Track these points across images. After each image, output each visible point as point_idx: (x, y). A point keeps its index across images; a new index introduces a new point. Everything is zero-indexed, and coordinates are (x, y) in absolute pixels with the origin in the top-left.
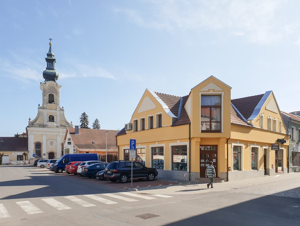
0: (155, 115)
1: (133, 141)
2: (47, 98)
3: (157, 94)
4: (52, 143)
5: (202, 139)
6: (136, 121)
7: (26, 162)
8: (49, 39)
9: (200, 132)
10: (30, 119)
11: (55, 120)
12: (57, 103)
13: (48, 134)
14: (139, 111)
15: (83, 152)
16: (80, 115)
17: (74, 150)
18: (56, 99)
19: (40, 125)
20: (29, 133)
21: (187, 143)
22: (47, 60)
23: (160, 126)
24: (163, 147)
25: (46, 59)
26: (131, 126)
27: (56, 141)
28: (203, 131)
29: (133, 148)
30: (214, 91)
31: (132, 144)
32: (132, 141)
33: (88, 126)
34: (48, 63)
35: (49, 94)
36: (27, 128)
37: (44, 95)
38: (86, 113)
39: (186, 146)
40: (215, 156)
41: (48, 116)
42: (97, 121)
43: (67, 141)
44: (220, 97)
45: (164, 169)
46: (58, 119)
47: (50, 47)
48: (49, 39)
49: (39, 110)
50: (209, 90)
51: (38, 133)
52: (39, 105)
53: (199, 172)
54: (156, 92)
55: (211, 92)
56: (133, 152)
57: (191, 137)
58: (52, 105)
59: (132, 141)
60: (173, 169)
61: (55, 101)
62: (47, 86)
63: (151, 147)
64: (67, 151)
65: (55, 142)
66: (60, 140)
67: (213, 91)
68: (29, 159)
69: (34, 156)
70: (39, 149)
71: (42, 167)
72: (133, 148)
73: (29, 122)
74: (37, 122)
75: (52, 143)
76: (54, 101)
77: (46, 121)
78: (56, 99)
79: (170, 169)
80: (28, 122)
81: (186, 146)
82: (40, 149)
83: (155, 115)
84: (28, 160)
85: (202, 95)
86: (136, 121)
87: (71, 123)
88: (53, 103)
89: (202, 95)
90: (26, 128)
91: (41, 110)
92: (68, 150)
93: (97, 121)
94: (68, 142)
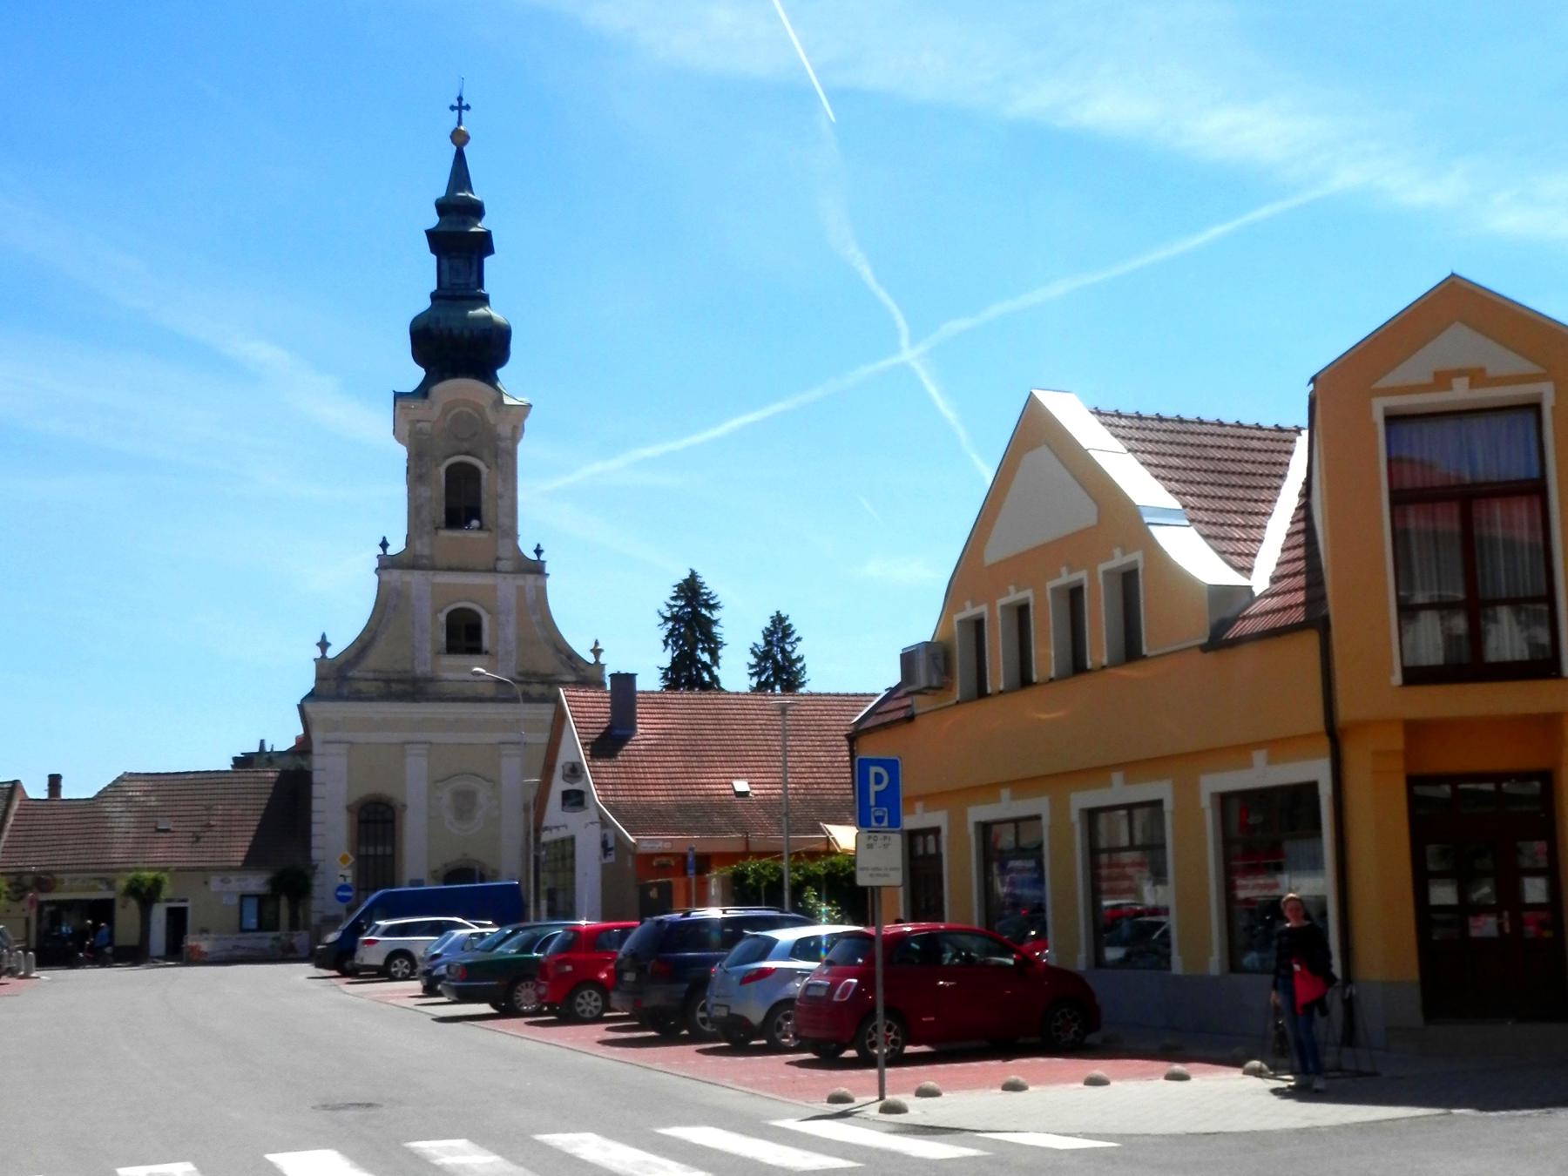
0: (1092, 577)
1: (881, 770)
2: (436, 490)
3: (1110, 418)
4: (465, 803)
5: (1415, 730)
6: (978, 624)
7: (295, 940)
8: (452, 108)
9: (1397, 678)
10: (324, 645)
11: (486, 642)
12: (504, 521)
13: (438, 737)
14: (992, 555)
15: (664, 860)
16: (661, 595)
17: (604, 844)
18: (499, 496)
19: (388, 681)
20: (317, 736)
21: (1317, 770)
22: (436, 239)
23: (1130, 650)
24: (1157, 804)
25: (431, 234)
26: (940, 662)
27: (494, 783)
28: (1415, 676)
29: (879, 820)
30: (1477, 377)
31: (874, 788)
32: (873, 770)
33: (715, 669)
34: (445, 262)
35: (449, 470)
36: (309, 707)
37: (416, 476)
38: (712, 583)
39: (1312, 787)
40: (1432, 849)
41: (442, 618)
42: (779, 630)
43: (559, 785)
44: (1531, 417)
45: (1178, 966)
46: (510, 632)
47: (460, 158)
48: (452, 108)
49: (386, 576)
50: (1442, 380)
51: (376, 737)
52: (384, 545)
53: (1413, 974)
54: (1108, 407)
55: (1460, 393)
56: (880, 843)
57: (1344, 713)
58: (470, 535)
59: (873, 770)
60: (1098, 961)
61: (487, 508)
62: (436, 412)
63: (1082, 811)
64: (564, 858)
65: (483, 794)
66: (516, 777)
67: (1472, 385)
68: (315, 919)
69: (342, 899)
70: (371, 851)
71: (400, 966)
72: (879, 820)
73: (321, 663)
74: (374, 660)
75: (465, 803)
76: (484, 508)
77: (427, 650)
78: (499, 496)
79: (1215, 964)
80: (313, 666)
81: (1312, 787)
82: (388, 850)
83: (1092, 577)
84: (306, 928)
85: (1392, 419)
86: (978, 624)
87: (590, 659)
88: (475, 523)
89: (1392, 419)
90: (301, 708)
91: (395, 575)
92: (568, 848)
93: (779, 630)
94: (566, 795)
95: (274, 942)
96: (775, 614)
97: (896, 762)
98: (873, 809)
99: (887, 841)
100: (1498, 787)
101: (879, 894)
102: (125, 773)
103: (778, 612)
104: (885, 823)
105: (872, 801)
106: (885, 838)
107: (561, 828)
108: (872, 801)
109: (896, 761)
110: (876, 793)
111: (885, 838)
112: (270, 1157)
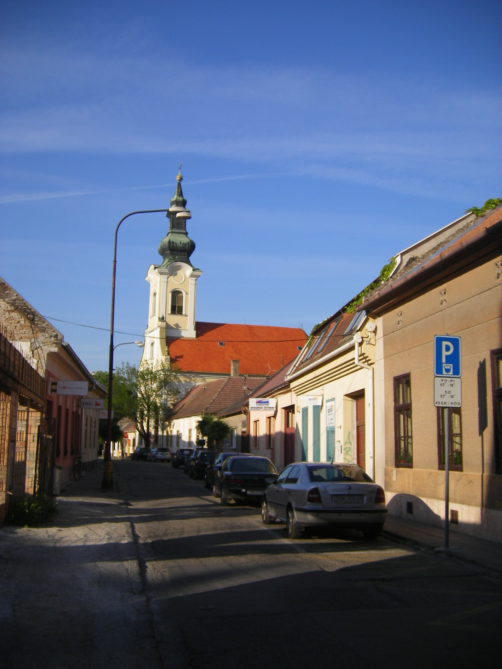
29: (448, 371)
31: (445, 353)
32: (444, 343)
56: (448, 383)
59: (444, 343)
72: (448, 371)
95: (136, 371)
96: (183, 357)
97: (437, 338)
98: (444, 365)
99: (452, 383)
100: (25, 397)
101: (334, 401)
102: (491, 199)
103: (486, 228)
104: (451, 372)
105: (444, 361)
106: (451, 381)
107: (41, 350)
108: (444, 361)
109: (437, 338)
110: (447, 356)
111: (451, 381)
112: (176, 217)
